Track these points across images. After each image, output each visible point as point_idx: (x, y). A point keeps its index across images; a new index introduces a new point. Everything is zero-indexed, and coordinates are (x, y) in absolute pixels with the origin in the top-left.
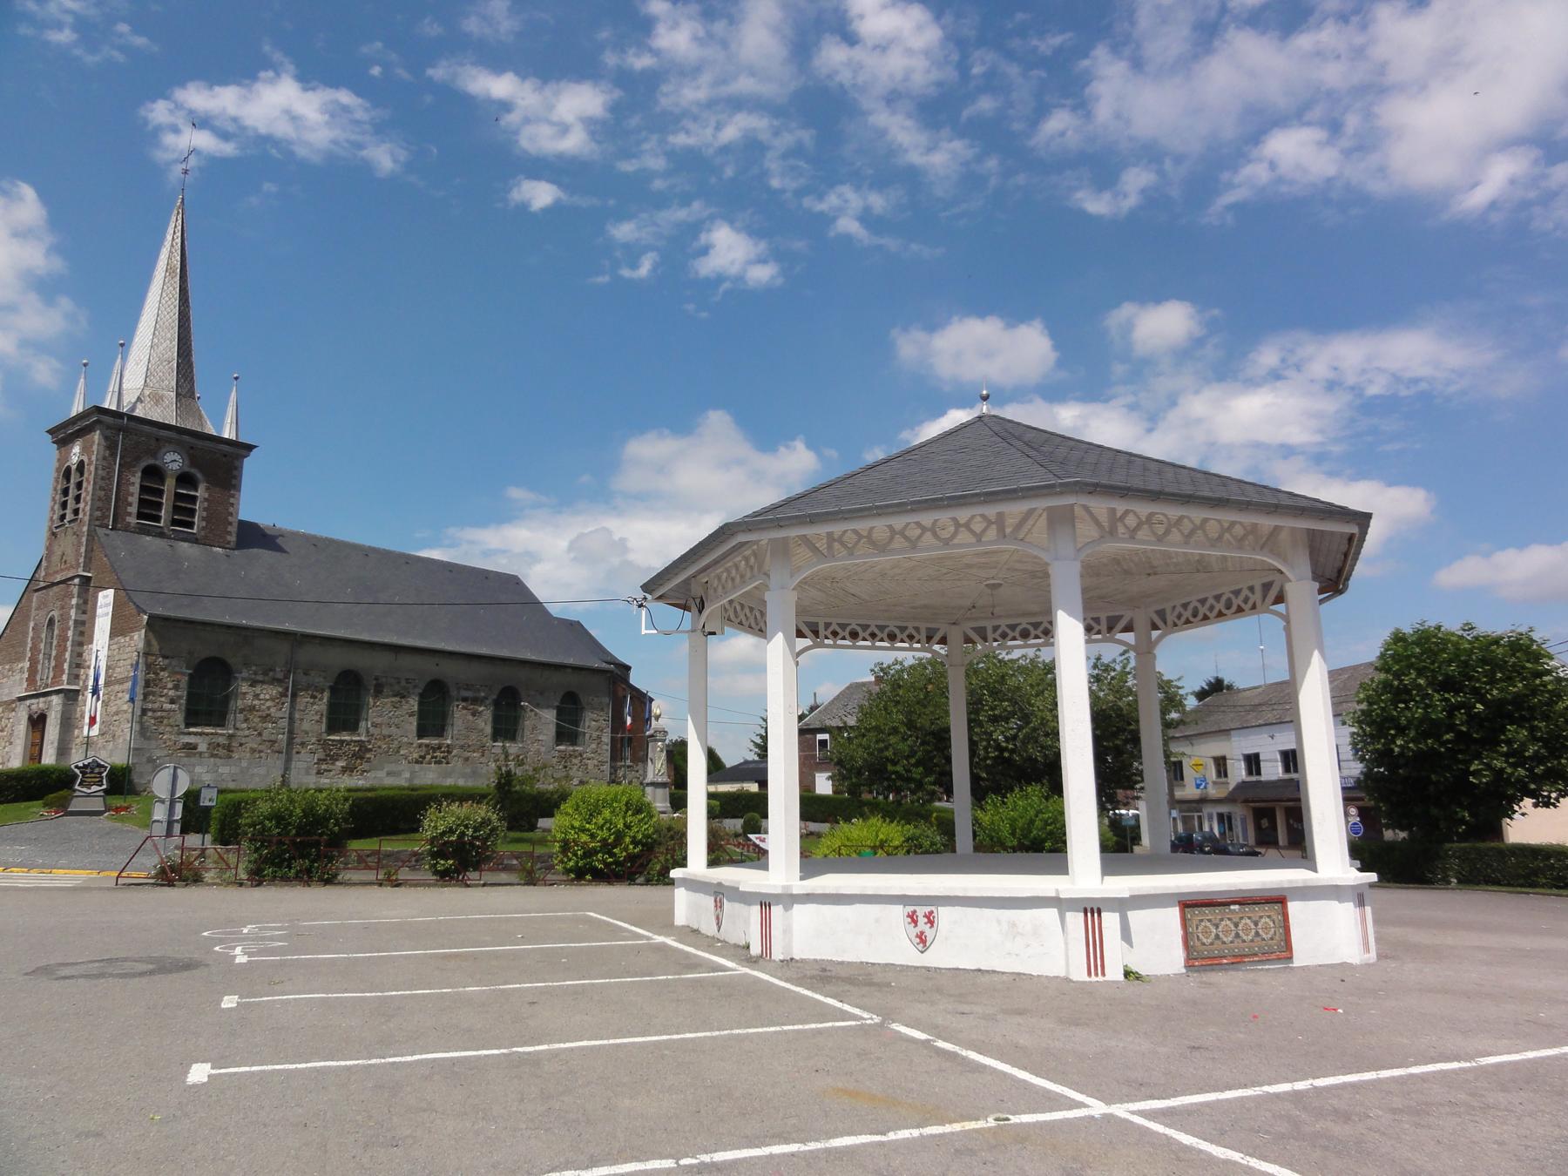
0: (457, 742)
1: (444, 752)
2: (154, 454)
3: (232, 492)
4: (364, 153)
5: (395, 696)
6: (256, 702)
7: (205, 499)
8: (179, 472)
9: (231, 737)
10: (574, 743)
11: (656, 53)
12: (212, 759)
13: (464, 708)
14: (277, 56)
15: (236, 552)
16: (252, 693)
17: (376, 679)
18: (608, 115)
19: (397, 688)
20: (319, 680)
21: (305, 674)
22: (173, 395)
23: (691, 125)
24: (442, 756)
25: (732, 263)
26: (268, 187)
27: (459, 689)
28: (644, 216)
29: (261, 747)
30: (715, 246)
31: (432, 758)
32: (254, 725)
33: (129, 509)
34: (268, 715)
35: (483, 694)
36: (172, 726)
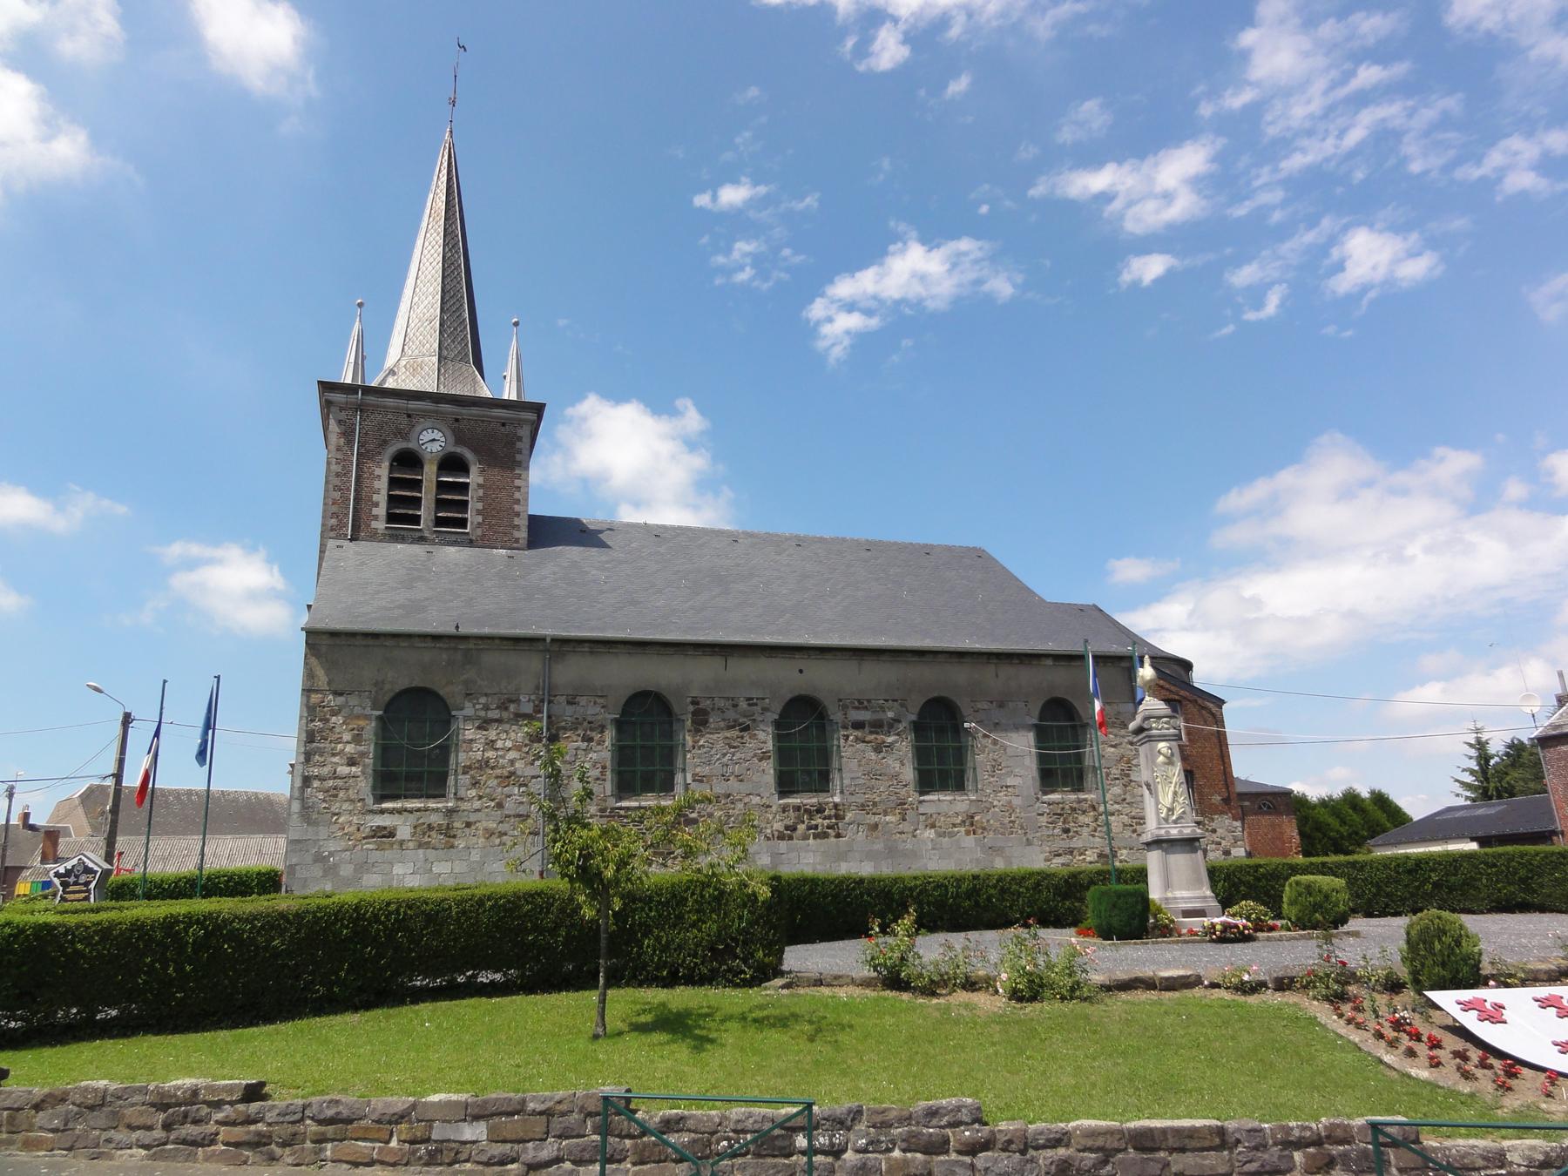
0: (852, 799)
1: (829, 817)
2: (405, 436)
3: (517, 472)
4: (986, 288)
5: (730, 728)
6: (491, 754)
7: (479, 485)
8: (441, 454)
9: (450, 812)
10: (1078, 786)
11: (1257, 84)
12: (421, 851)
13: (857, 739)
14: (902, 227)
15: (526, 552)
16: (483, 741)
17: (694, 703)
18: (1214, 167)
19: (731, 714)
20: (591, 709)
21: (569, 703)
22: (435, 359)
23: (1305, 142)
24: (830, 825)
25: (1374, 268)
26: (907, 343)
27: (845, 707)
28: (1264, 253)
29: (504, 827)
30: (1350, 256)
31: (809, 828)
32: (488, 790)
33: (375, 511)
34: (512, 774)
35: (890, 714)
36: (352, 801)
